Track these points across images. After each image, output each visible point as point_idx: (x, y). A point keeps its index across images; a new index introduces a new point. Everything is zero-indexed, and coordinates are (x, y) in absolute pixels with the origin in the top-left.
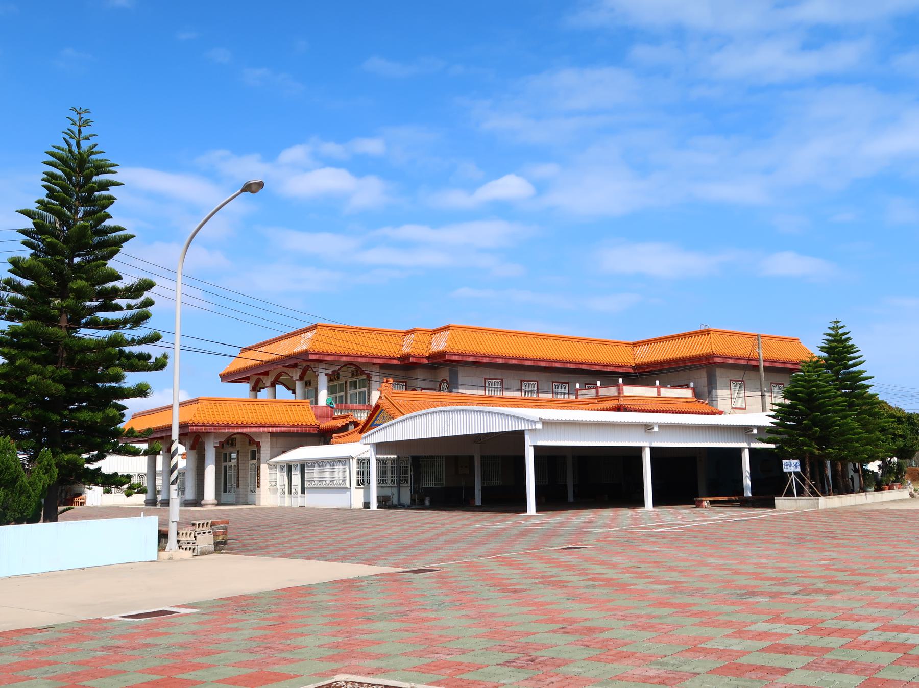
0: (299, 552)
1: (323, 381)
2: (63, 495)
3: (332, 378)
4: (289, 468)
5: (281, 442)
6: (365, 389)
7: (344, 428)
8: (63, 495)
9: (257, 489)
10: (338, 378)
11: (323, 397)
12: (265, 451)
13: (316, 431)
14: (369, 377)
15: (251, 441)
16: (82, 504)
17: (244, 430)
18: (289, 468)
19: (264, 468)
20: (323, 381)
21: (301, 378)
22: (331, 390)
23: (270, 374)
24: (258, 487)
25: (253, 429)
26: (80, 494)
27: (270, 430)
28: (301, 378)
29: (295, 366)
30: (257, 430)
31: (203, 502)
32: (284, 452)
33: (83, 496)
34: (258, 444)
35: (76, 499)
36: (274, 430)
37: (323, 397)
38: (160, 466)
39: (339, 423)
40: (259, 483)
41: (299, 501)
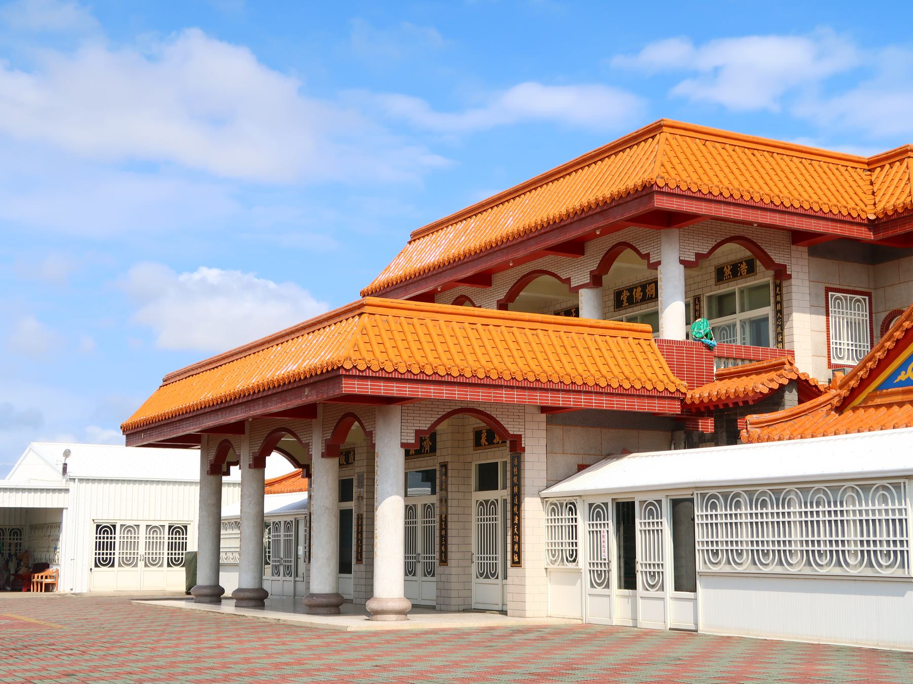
0: (402, 639)
1: (390, 464)
2: (12, 566)
3: (420, 448)
4: (625, 513)
5: (577, 439)
6: (768, 311)
7: (770, 401)
8: (12, 566)
9: (511, 571)
10: (433, 449)
11: (673, 320)
12: (535, 463)
13: (675, 408)
14: (781, 274)
15: (491, 433)
16: (49, 588)
17: (478, 396)
18: (625, 513)
19: (533, 511)
20: (390, 464)
21: (596, 281)
22: (693, 312)
23: (497, 279)
24: (517, 563)
25: (503, 395)
26: (45, 566)
27: (549, 400)
28: (596, 281)
29: (575, 248)
30: (516, 396)
31: (372, 605)
32: (582, 468)
33: (52, 569)
34: (516, 446)
35: (37, 578)
36: (561, 400)
37: (673, 320)
38: (232, 503)
39: (762, 384)
40: (517, 553)
41: (661, 609)
